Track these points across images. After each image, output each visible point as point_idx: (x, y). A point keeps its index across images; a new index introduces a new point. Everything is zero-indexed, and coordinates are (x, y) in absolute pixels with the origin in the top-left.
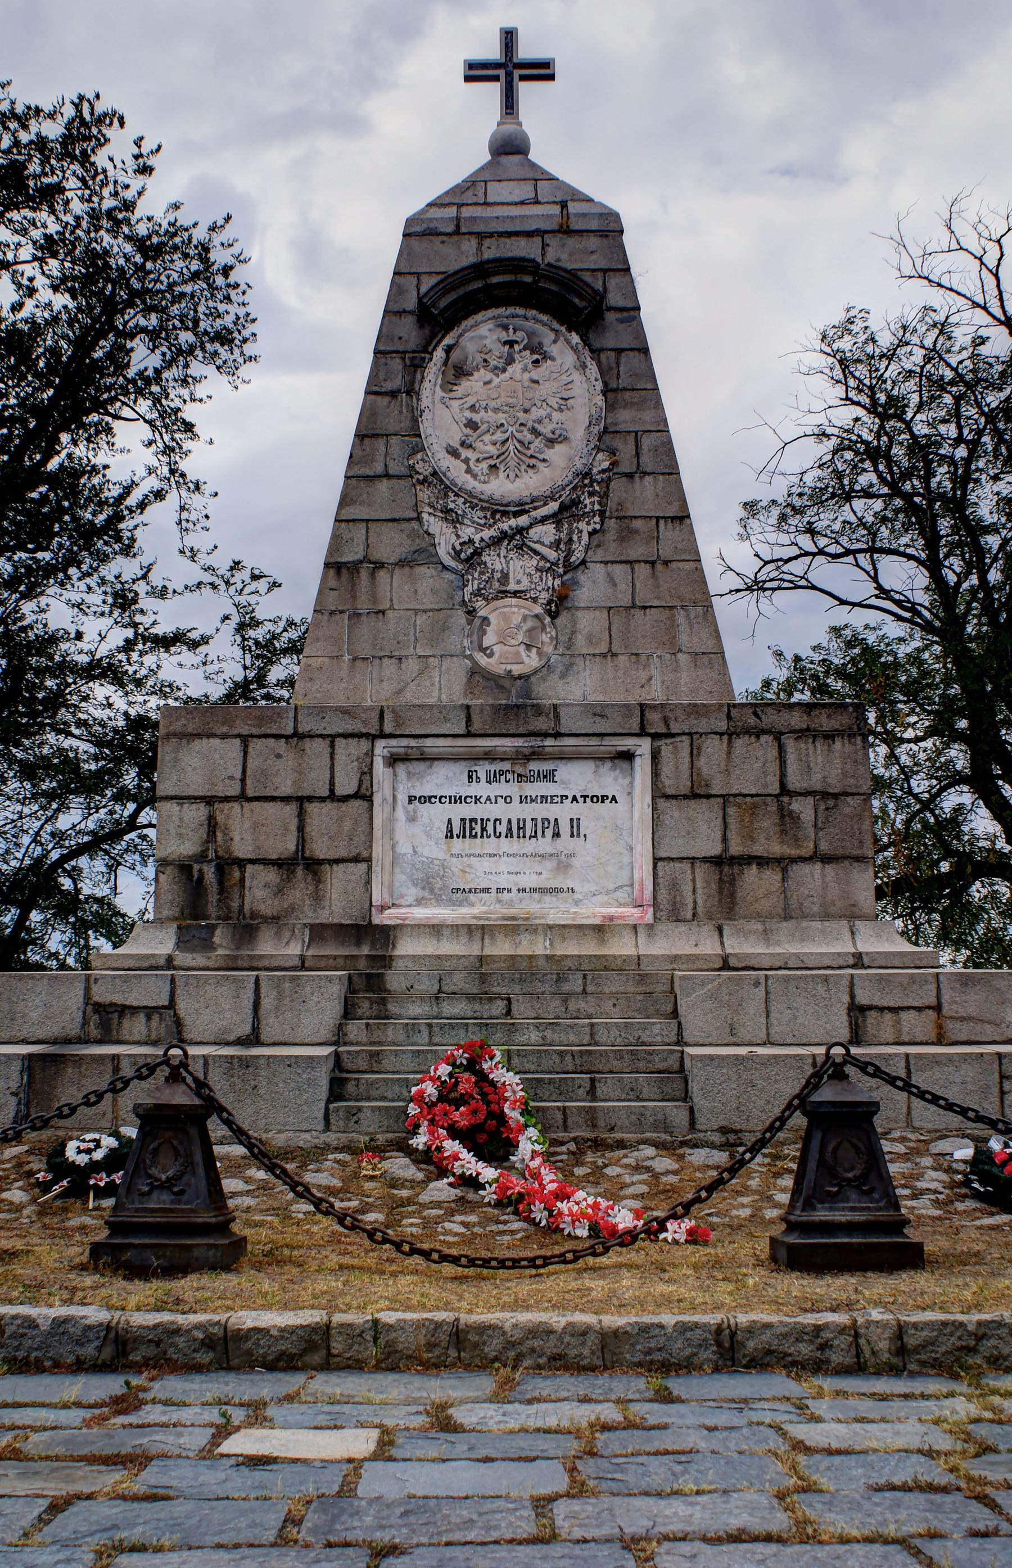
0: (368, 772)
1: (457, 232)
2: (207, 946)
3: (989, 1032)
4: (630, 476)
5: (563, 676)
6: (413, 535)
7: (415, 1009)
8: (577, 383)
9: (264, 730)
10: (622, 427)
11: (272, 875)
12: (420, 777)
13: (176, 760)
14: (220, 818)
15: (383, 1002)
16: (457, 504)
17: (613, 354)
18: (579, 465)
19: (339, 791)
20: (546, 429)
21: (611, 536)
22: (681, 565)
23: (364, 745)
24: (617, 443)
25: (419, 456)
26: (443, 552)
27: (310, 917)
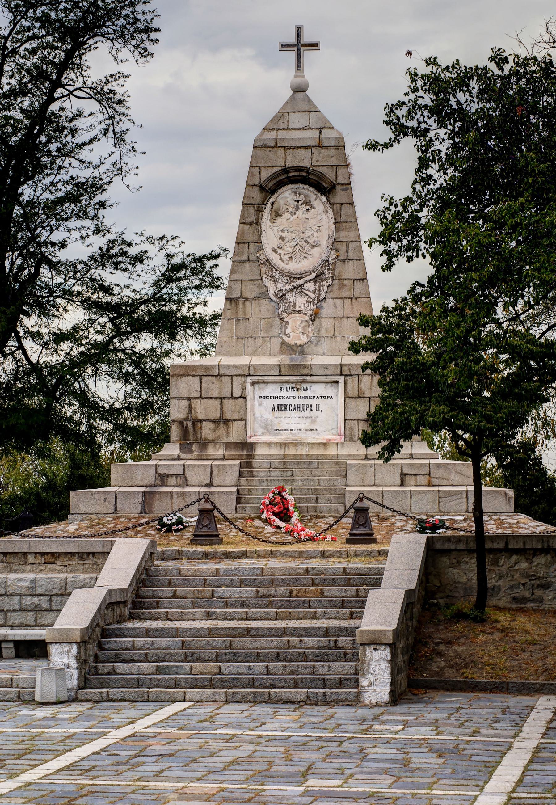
0: (244, 389)
1: (276, 146)
2: (191, 451)
3: (445, 482)
4: (344, 261)
5: (316, 345)
6: (259, 286)
7: (262, 474)
8: (324, 219)
9: (207, 373)
10: (341, 239)
11: (211, 425)
12: (263, 389)
13: (176, 384)
14: (193, 405)
15: (252, 471)
16: (276, 274)
17: (339, 206)
18: (324, 257)
19: (235, 395)
20: (311, 241)
21: (336, 287)
22: (362, 299)
23: (243, 379)
24: (339, 246)
25: (261, 252)
26: (271, 294)
27: (225, 440)
